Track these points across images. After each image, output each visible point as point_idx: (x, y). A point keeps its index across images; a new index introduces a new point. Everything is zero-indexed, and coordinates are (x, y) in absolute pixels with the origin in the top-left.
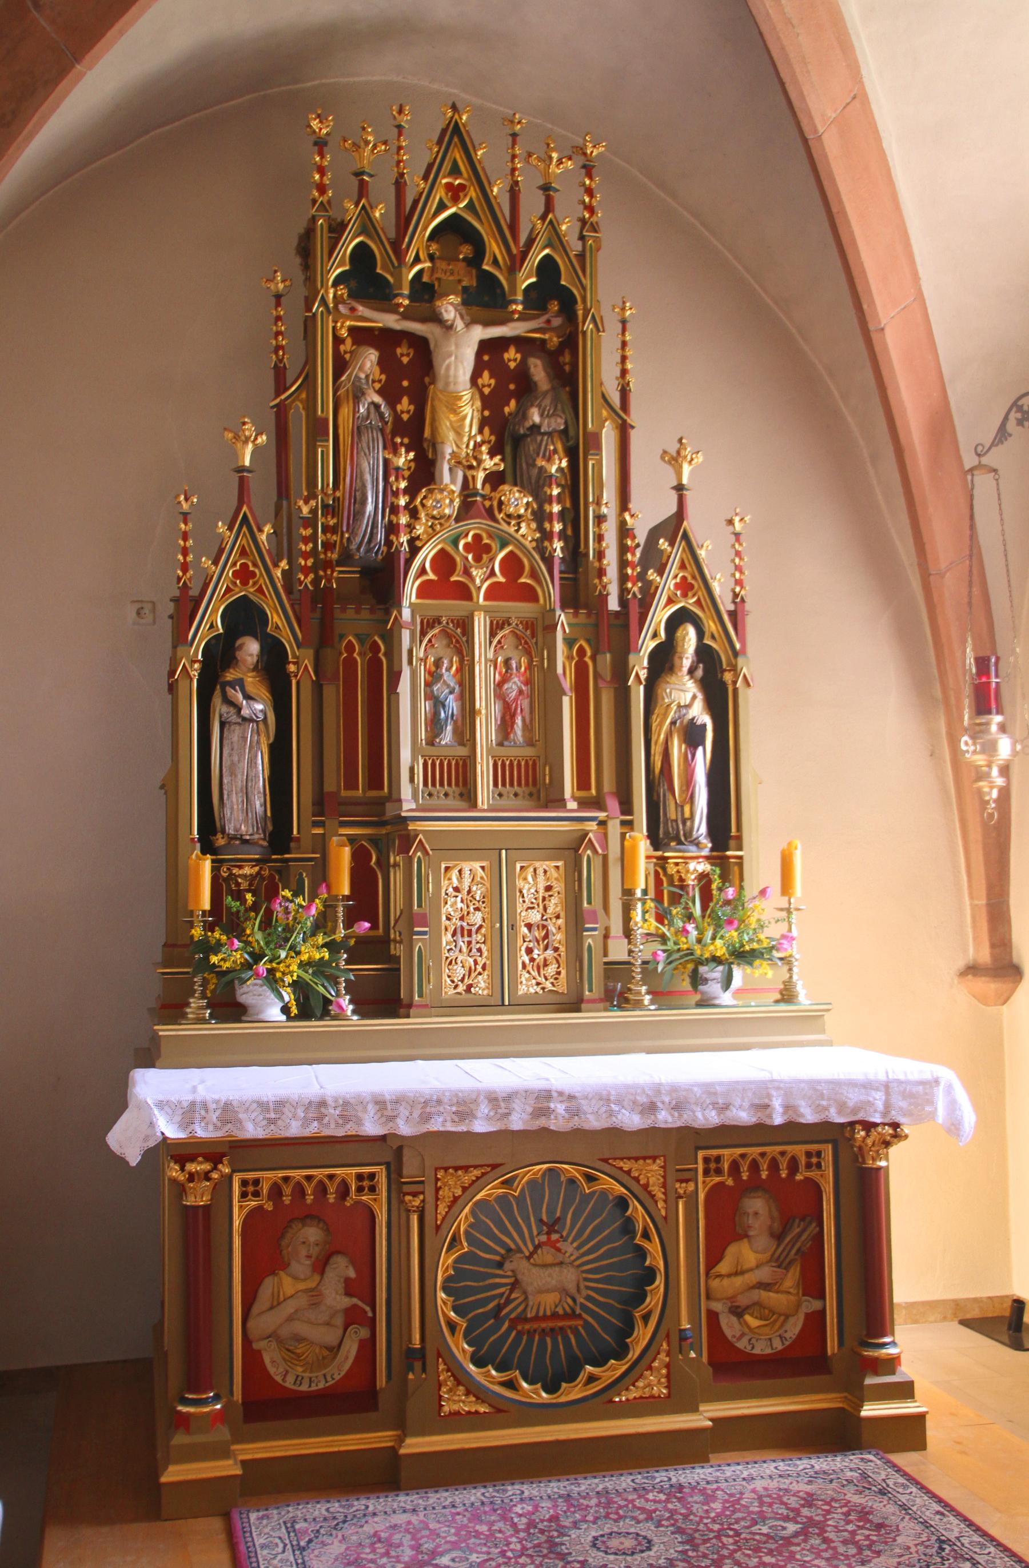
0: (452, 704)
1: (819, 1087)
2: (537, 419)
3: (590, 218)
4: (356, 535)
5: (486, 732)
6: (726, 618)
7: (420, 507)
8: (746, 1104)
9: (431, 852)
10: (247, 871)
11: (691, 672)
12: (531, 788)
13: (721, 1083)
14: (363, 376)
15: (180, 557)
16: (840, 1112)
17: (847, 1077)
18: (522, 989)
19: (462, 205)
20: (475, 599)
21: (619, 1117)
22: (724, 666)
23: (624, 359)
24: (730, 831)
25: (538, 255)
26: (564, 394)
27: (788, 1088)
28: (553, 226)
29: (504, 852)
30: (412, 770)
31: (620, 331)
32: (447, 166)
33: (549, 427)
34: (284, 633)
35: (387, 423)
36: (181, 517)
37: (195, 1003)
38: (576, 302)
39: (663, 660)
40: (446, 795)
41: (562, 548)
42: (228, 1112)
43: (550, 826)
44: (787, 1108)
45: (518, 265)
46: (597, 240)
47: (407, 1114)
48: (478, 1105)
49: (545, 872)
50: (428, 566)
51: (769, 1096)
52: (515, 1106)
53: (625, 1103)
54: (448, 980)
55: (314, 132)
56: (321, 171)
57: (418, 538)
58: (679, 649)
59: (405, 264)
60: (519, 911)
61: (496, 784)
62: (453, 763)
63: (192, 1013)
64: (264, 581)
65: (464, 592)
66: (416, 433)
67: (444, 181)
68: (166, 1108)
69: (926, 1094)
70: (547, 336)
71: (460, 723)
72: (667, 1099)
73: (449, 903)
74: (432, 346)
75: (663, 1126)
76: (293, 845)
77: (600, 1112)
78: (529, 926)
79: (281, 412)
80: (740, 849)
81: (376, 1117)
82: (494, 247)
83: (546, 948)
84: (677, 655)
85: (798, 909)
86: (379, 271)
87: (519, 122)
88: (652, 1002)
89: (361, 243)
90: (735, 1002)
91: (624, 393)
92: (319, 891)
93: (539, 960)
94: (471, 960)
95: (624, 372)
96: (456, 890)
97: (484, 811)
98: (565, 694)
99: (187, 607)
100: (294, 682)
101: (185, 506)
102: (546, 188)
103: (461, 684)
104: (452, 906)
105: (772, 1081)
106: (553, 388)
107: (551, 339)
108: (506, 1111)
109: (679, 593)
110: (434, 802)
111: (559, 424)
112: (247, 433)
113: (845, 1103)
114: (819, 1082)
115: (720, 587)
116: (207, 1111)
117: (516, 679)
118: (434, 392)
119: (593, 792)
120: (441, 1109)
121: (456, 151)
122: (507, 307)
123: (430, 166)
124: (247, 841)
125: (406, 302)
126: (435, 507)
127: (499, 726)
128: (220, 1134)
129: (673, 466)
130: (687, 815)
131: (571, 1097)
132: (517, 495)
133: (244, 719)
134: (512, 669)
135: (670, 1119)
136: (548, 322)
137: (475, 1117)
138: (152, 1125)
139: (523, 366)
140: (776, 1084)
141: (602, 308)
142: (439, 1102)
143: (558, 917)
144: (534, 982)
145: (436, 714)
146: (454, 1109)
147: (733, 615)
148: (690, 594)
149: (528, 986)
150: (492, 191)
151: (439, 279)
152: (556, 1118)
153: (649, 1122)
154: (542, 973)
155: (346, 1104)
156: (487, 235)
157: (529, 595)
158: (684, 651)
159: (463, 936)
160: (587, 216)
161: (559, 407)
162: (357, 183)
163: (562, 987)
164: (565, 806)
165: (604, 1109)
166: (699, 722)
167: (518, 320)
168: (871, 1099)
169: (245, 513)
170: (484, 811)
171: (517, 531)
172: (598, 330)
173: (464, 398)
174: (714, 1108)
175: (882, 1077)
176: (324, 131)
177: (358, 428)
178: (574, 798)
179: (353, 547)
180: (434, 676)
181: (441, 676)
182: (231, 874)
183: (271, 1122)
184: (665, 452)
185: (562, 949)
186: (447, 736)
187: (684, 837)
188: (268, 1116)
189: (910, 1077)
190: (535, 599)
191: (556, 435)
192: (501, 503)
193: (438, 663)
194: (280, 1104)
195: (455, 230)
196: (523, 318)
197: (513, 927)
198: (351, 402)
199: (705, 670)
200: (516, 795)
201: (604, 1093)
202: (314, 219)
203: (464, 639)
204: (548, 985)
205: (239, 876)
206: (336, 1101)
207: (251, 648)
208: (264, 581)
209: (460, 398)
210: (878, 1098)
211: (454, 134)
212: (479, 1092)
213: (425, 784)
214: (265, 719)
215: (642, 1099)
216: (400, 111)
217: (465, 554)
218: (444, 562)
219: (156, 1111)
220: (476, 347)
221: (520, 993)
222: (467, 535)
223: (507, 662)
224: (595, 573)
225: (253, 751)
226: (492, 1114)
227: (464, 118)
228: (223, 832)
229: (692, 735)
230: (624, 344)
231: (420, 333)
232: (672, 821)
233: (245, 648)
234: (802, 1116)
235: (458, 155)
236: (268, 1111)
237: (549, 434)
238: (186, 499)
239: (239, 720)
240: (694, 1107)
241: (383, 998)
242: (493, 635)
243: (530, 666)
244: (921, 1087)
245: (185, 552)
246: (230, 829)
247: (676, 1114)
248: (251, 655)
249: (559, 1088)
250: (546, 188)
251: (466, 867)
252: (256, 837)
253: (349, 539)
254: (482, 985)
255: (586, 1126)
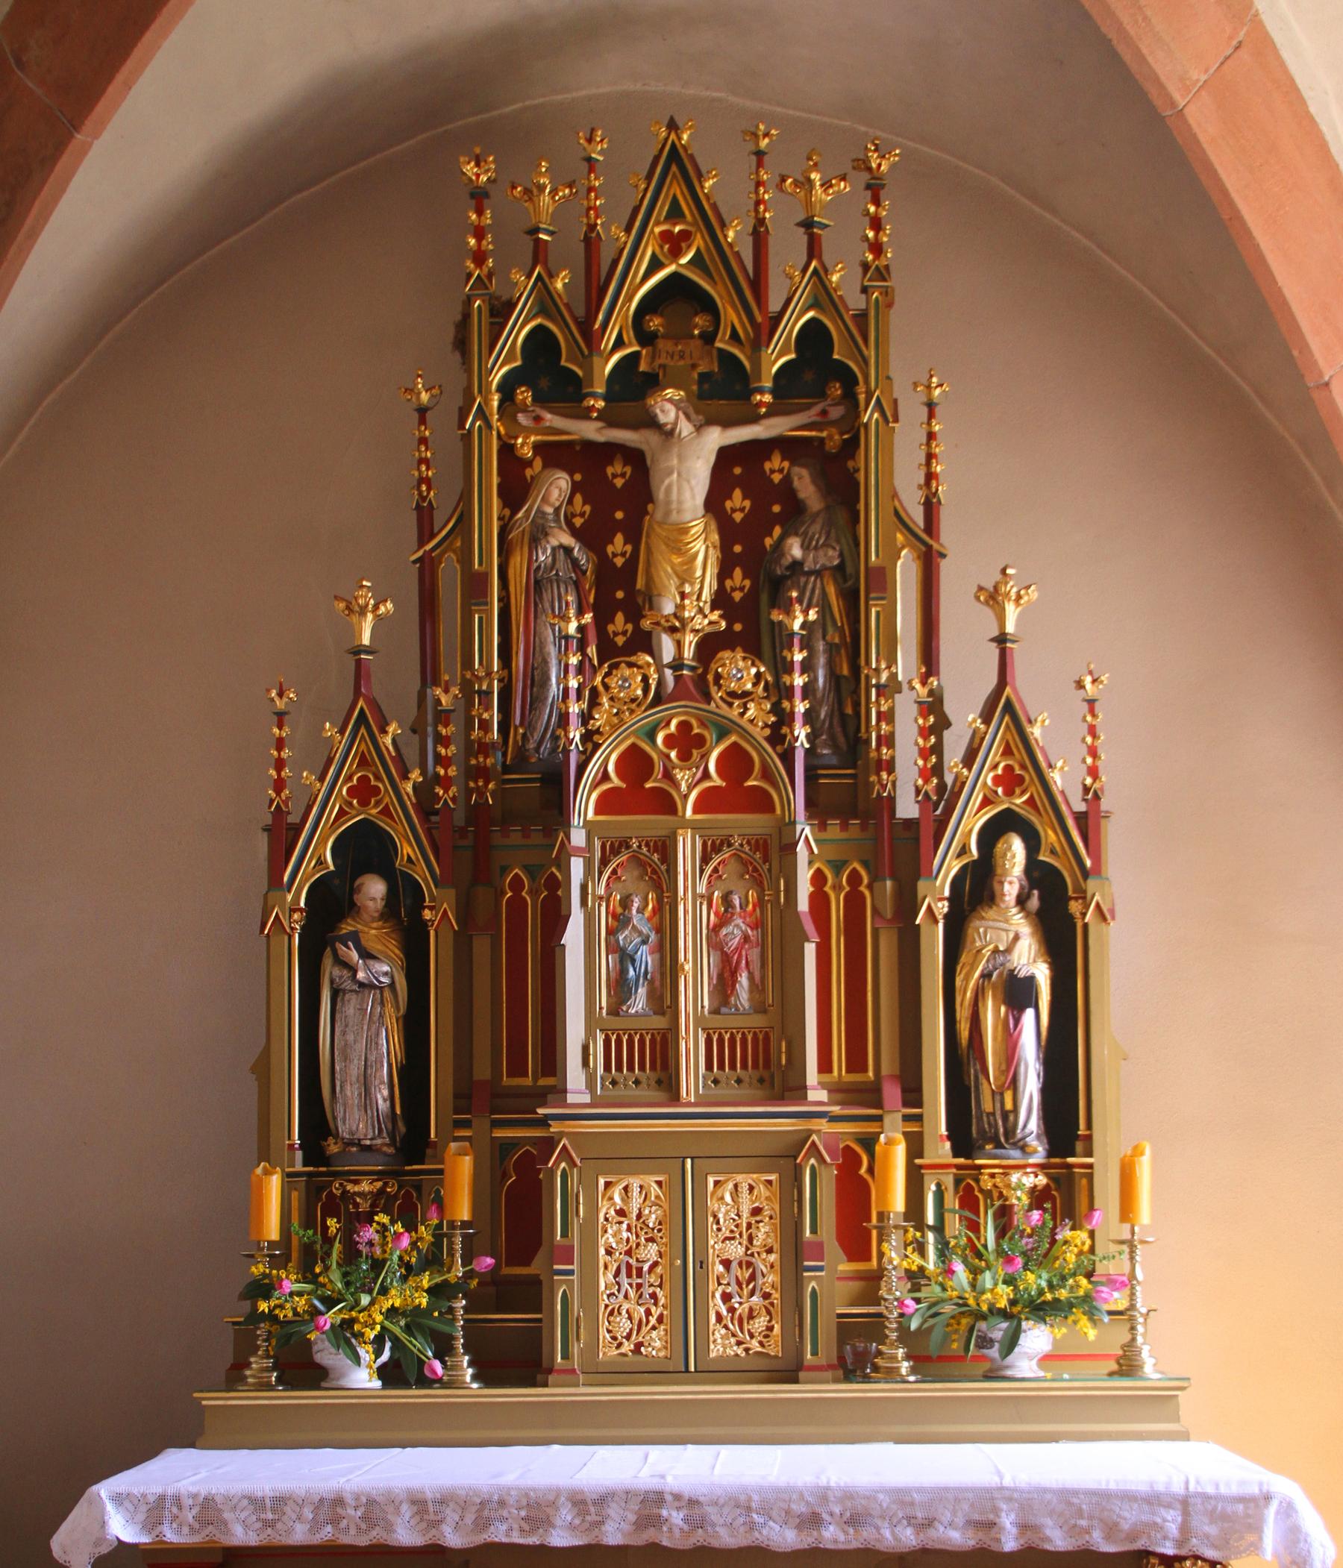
0: (646, 957)
1: (1075, 1501)
2: (797, 552)
3: (874, 260)
4: (535, 729)
5: (694, 995)
6: (1070, 823)
7: (601, 688)
8: (960, 1520)
9: (578, 1162)
10: (365, 1186)
11: (1021, 901)
12: (659, 1073)
13: (920, 1490)
14: (550, 510)
15: (273, 772)
16: (1108, 1537)
17: (1122, 1487)
18: (715, 1351)
19: (684, 261)
20: (680, 813)
21: (765, 1532)
22: (1070, 893)
23: (930, 457)
24: (1078, 1129)
25: (795, 323)
26: (841, 517)
27: (1027, 1501)
28: (820, 277)
29: (689, 1161)
30: (585, 1049)
31: (925, 419)
32: (663, 208)
33: (815, 563)
34: (418, 868)
35: (584, 573)
36: (275, 718)
37: (256, 1363)
38: (857, 383)
39: (976, 889)
40: (637, 1082)
41: (808, 736)
42: (209, 1509)
43: (757, 1125)
44: (1024, 1527)
45: (764, 338)
46: (886, 292)
47: (457, 1519)
48: (557, 1509)
49: (751, 1188)
50: (611, 768)
51: (996, 1511)
52: (611, 1512)
53: (774, 1514)
54: (608, 1336)
55: (470, 180)
56: (479, 233)
57: (598, 731)
58: (999, 871)
59: (600, 353)
60: (711, 1242)
61: (709, 1066)
62: (648, 1038)
63: (253, 1376)
64: (389, 798)
65: (665, 803)
66: (620, 603)
67: (657, 230)
68: (127, 1503)
69: (1248, 1516)
70: (824, 434)
71: (657, 983)
72: (837, 1510)
73: (610, 1231)
74: (649, 462)
75: (830, 1546)
76: (429, 1151)
77: (736, 1524)
78: (727, 1264)
79: (427, 568)
80: (1090, 1154)
81: (413, 1522)
82: (731, 316)
83: (752, 1293)
84: (997, 878)
85: (1143, 1242)
86: (563, 363)
87: (766, 135)
88: (913, 1370)
89: (540, 327)
90: (1041, 1374)
91: (931, 507)
92: (429, 1215)
93: (742, 1310)
94: (642, 1310)
95: (930, 476)
96: (612, 1217)
97: (689, 1104)
98: (808, 941)
99: (283, 836)
100: (432, 933)
101: (280, 704)
102: (808, 224)
103: (659, 930)
104: (614, 1235)
105: (1001, 1488)
106: (827, 508)
107: (831, 437)
108: (599, 1518)
109: (1000, 790)
110: (620, 1092)
111: (831, 559)
112: (361, 601)
113: (1116, 1524)
114: (1075, 1492)
115: (1064, 778)
116: (180, 1508)
117: (739, 921)
118: (650, 526)
119: (871, 1074)
120: (505, 1514)
121: (675, 186)
122: (581, 401)
123: (636, 210)
124: (369, 1148)
125: (601, 404)
126: (622, 688)
127: (715, 987)
128: (197, 1539)
129: (991, 607)
130: (1009, 1106)
131: (693, 1503)
132: (741, 664)
133: (361, 985)
134: (733, 907)
135: (842, 1537)
136: (824, 413)
137: (554, 1527)
138: (103, 1524)
139: (787, 480)
140: (1007, 1493)
141: (896, 388)
142: (502, 1503)
143: (770, 1251)
144: (733, 1340)
145: (623, 972)
146: (523, 1513)
147: (1081, 818)
148: (1018, 791)
149: (724, 1347)
150: (726, 237)
151: (663, 366)
152: (670, 1530)
153: (810, 1540)
154: (746, 1327)
155: (371, 1502)
156: (721, 297)
157: (761, 802)
158: (1006, 873)
159: (629, 1276)
160: (870, 257)
161: (833, 534)
162: (532, 244)
163: (774, 1349)
164: (805, 1097)
165: (741, 1520)
166: (1022, 974)
167: (597, 419)
168: (1159, 1520)
169: (362, 709)
170: (689, 1104)
171: (742, 714)
172: (887, 422)
173: (693, 532)
174: (909, 1524)
175: (1178, 1488)
176: (484, 178)
177: (537, 582)
178: (822, 1085)
179: (531, 745)
180: (620, 920)
181: (629, 920)
182: (345, 1192)
183: (268, 1524)
184: (981, 589)
185: (776, 1295)
186: (639, 1002)
187: (1008, 1136)
188: (263, 1516)
189: (1223, 1490)
190: (771, 809)
191: (827, 573)
192: (718, 677)
193: (626, 903)
194: (280, 1502)
195: (675, 294)
196: (773, 411)
197: (702, 1264)
198: (526, 549)
199: (1041, 898)
200: (739, 1081)
201: (743, 1498)
202: (469, 301)
203: (663, 868)
204: (755, 1345)
205: (355, 1193)
206: (357, 1499)
207: (374, 889)
208: (389, 798)
209: (685, 531)
210: (1171, 1521)
211: (676, 162)
212: (558, 1492)
213: (607, 1067)
214: (392, 985)
215: (799, 1508)
216: (590, 140)
217: (665, 750)
218: (635, 763)
219: (110, 1507)
220: (713, 459)
221: (713, 1355)
222: (668, 724)
223: (726, 899)
224: (873, 767)
225: (374, 1027)
226: (577, 1522)
227: (685, 137)
228: (336, 1136)
229: (1018, 993)
230: (931, 436)
231: (633, 445)
232: (988, 1114)
233: (364, 889)
234: (1049, 1540)
235: (675, 189)
236: (263, 1508)
237: (818, 573)
238: (280, 695)
239: (356, 987)
240: (879, 1522)
241: (516, 1358)
242: (705, 860)
243: (760, 903)
244: (1240, 1507)
245: (280, 764)
246: (344, 1131)
247: (851, 1531)
248: (374, 899)
249: (676, 1490)
250: (808, 224)
251: (635, 1182)
252: (379, 1141)
253: (524, 735)
254: (656, 1343)
255: (715, 1543)
